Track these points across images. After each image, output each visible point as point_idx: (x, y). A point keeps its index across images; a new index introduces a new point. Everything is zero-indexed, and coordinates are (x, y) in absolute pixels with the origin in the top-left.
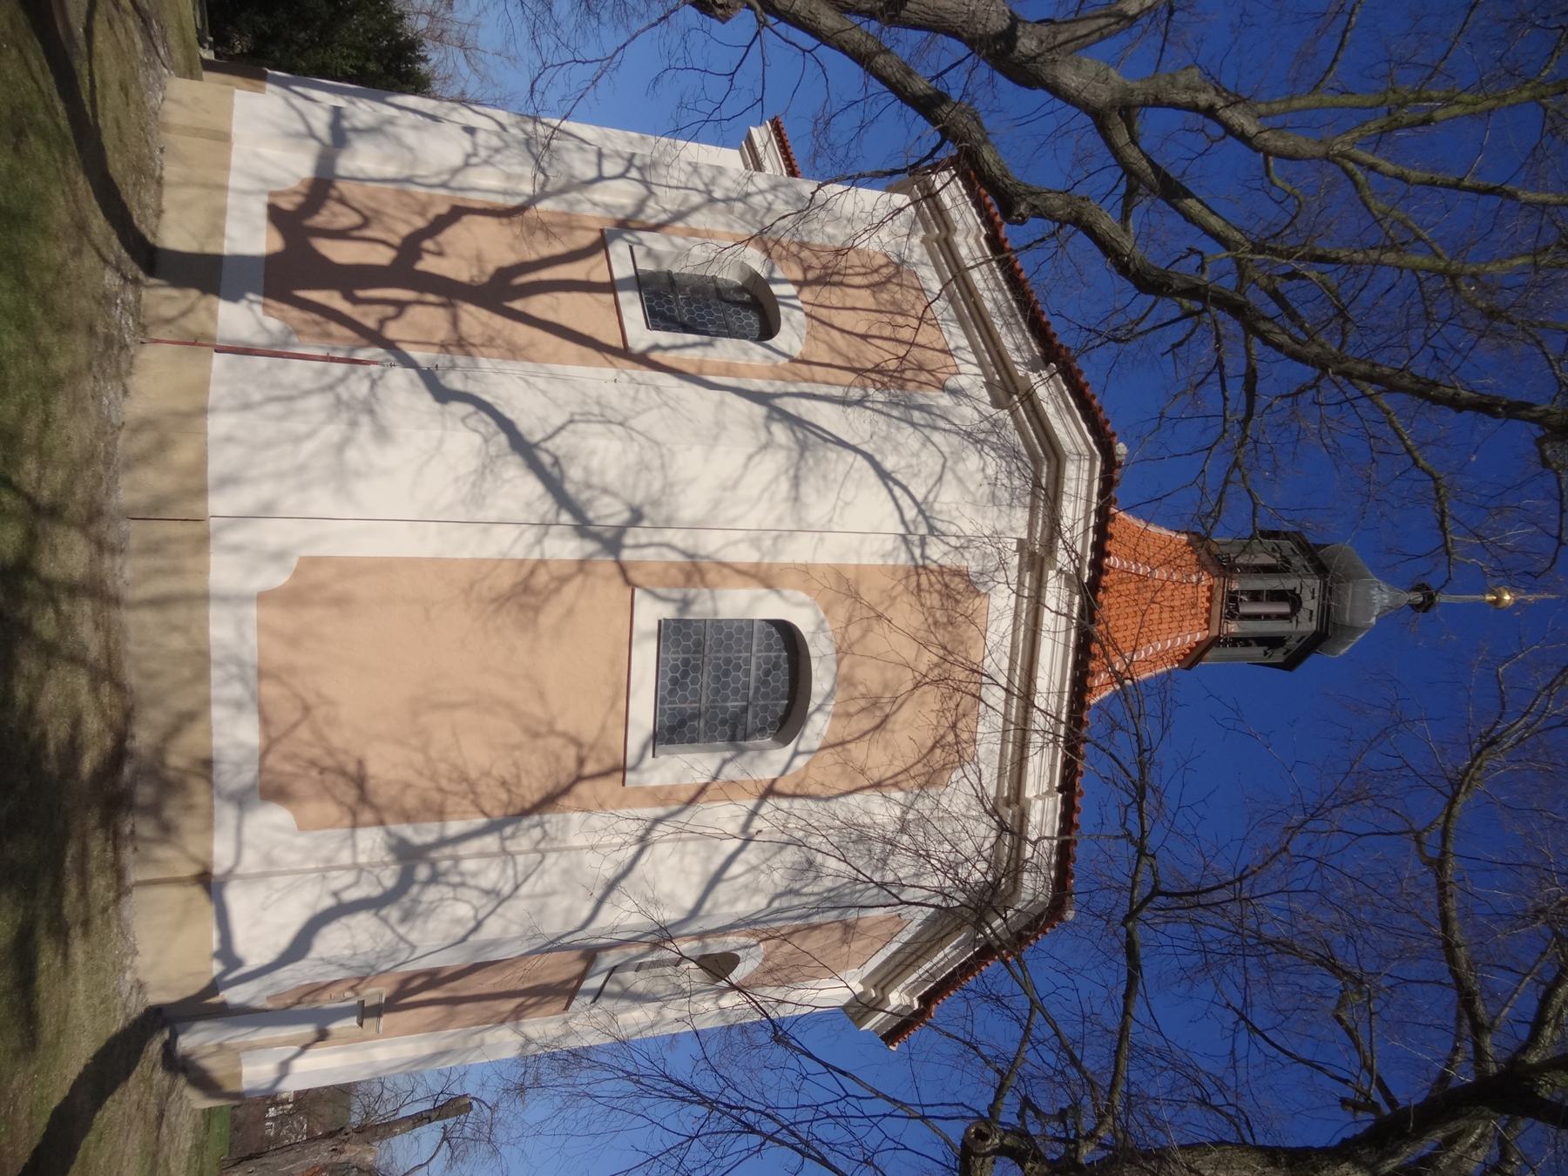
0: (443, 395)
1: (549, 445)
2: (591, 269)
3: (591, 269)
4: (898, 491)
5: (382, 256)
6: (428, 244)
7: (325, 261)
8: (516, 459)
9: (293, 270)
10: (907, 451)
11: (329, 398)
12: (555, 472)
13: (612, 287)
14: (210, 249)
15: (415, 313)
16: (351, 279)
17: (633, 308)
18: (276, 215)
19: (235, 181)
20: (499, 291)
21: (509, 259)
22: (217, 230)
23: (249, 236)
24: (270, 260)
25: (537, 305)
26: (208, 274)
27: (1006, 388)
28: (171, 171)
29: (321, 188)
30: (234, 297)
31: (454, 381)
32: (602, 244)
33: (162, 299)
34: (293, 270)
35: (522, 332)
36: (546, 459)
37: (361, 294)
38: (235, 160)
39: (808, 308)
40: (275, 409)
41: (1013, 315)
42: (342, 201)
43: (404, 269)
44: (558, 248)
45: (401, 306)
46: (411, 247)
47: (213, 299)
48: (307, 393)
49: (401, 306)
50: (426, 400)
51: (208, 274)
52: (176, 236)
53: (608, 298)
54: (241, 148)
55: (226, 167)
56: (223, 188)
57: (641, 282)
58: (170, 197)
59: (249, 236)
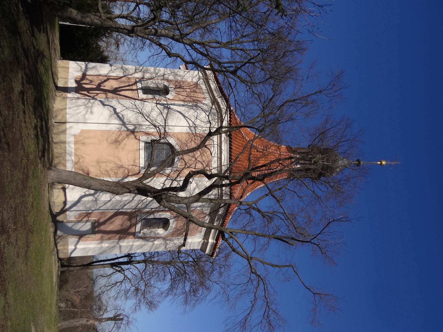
0: (104, 105)
1: (122, 113)
2: (134, 87)
3: (134, 87)
4: (188, 120)
5: (94, 87)
6: (102, 85)
7: (84, 87)
8: (115, 116)
9: (79, 88)
10: (191, 113)
11: (85, 106)
12: (122, 118)
13: (137, 90)
14: (65, 86)
15: (100, 95)
16: (88, 90)
17: (140, 92)
18: (76, 81)
19: (69, 77)
20: (115, 91)
21: (117, 86)
22: (66, 83)
23: (72, 84)
24: (76, 87)
25: (122, 93)
26: (66, 90)
27: (214, 101)
28: (59, 76)
29: (84, 76)
30: (70, 93)
31: (107, 103)
32: (136, 83)
33: (59, 94)
34: (79, 88)
35: (119, 96)
36: (121, 116)
37: (90, 92)
38: (69, 75)
39: (176, 92)
40: (75, 108)
41: (214, 82)
42: (87, 79)
43: (98, 88)
44: (126, 85)
45: (98, 94)
46: (100, 85)
47: (66, 93)
48: (81, 106)
49: (98, 94)
50: (102, 106)
51: (66, 90)
52: (60, 84)
53: (136, 91)
54: (70, 71)
55: (68, 76)
56: (68, 79)
57: (141, 89)
58: (60, 80)
59: (72, 84)
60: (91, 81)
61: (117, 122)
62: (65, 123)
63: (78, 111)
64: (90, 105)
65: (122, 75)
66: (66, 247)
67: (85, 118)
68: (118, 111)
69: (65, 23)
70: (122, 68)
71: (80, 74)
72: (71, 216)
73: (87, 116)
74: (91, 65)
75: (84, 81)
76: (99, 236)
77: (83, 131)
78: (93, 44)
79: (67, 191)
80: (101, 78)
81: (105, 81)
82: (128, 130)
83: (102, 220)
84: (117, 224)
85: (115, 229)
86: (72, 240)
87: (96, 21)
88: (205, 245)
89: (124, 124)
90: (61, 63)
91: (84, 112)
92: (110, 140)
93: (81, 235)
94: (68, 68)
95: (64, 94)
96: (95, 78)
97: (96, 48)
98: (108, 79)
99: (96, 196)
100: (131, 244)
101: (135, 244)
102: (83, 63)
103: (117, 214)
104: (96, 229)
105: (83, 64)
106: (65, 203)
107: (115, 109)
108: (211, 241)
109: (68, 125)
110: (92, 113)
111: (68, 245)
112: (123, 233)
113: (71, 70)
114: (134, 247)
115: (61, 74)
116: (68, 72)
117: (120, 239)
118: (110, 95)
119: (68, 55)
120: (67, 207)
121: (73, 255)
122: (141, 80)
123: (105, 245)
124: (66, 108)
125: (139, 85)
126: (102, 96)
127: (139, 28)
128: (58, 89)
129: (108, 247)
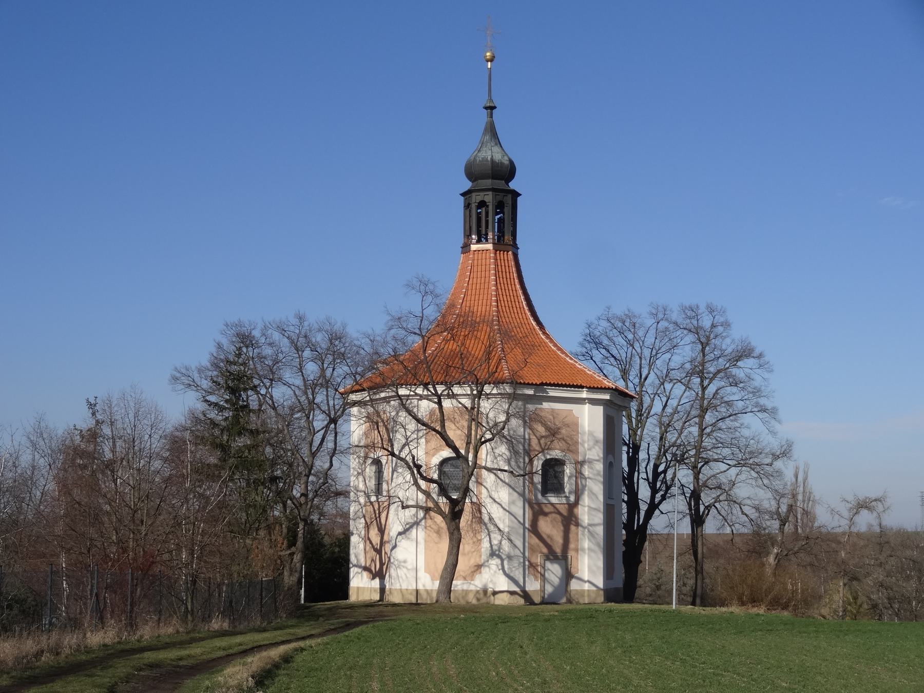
2: (376, 506)
9: (380, 574)
16: (382, 564)
18: (373, 578)
23: (376, 583)
26: (382, 590)
29: (366, 569)
31: (394, 542)
34: (380, 574)
43: (379, 552)
46: (375, 550)
51: (382, 590)
52: (377, 597)
54: (361, 585)
60: (372, 560)
61: (414, 531)
62: (417, 591)
63: (404, 577)
64: (396, 563)
65: (363, 520)
66: (586, 594)
67: (412, 569)
68: (400, 529)
69: (303, 596)
70: (354, 520)
71: (365, 574)
72: (533, 586)
73: (409, 567)
74: (353, 558)
75: (373, 569)
76: (571, 554)
77: (427, 570)
78: (334, 553)
79: (497, 589)
80: (368, 548)
81: (371, 543)
82: (425, 518)
83: (545, 550)
84: (550, 528)
85: (561, 534)
86: (574, 585)
87: (299, 557)
88: (593, 402)
89: (417, 523)
90: (353, 598)
91: (405, 570)
92: (437, 540)
93: (568, 575)
94: (358, 588)
95: (387, 592)
96: (368, 556)
97: (339, 546)
98: (369, 539)
99: (504, 557)
100: (586, 509)
101: (587, 504)
102: (352, 570)
103: (534, 529)
104: (561, 556)
105: (353, 571)
106: (512, 593)
107: (400, 534)
108: (584, 394)
109: (420, 587)
110: (405, 562)
111: (584, 591)
112: (569, 520)
113: (361, 585)
114: (593, 506)
115: (366, 597)
116: (364, 588)
117: (577, 524)
118: (386, 538)
119: (342, 588)
120: (517, 590)
121: (601, 585)
122: (368, 496)
123: (586, 544)
124: (401, 590)
125: (373, 499)
126: (388, 547)
127: (302, 514)
128: (382, 599)
129: (589, 540)
